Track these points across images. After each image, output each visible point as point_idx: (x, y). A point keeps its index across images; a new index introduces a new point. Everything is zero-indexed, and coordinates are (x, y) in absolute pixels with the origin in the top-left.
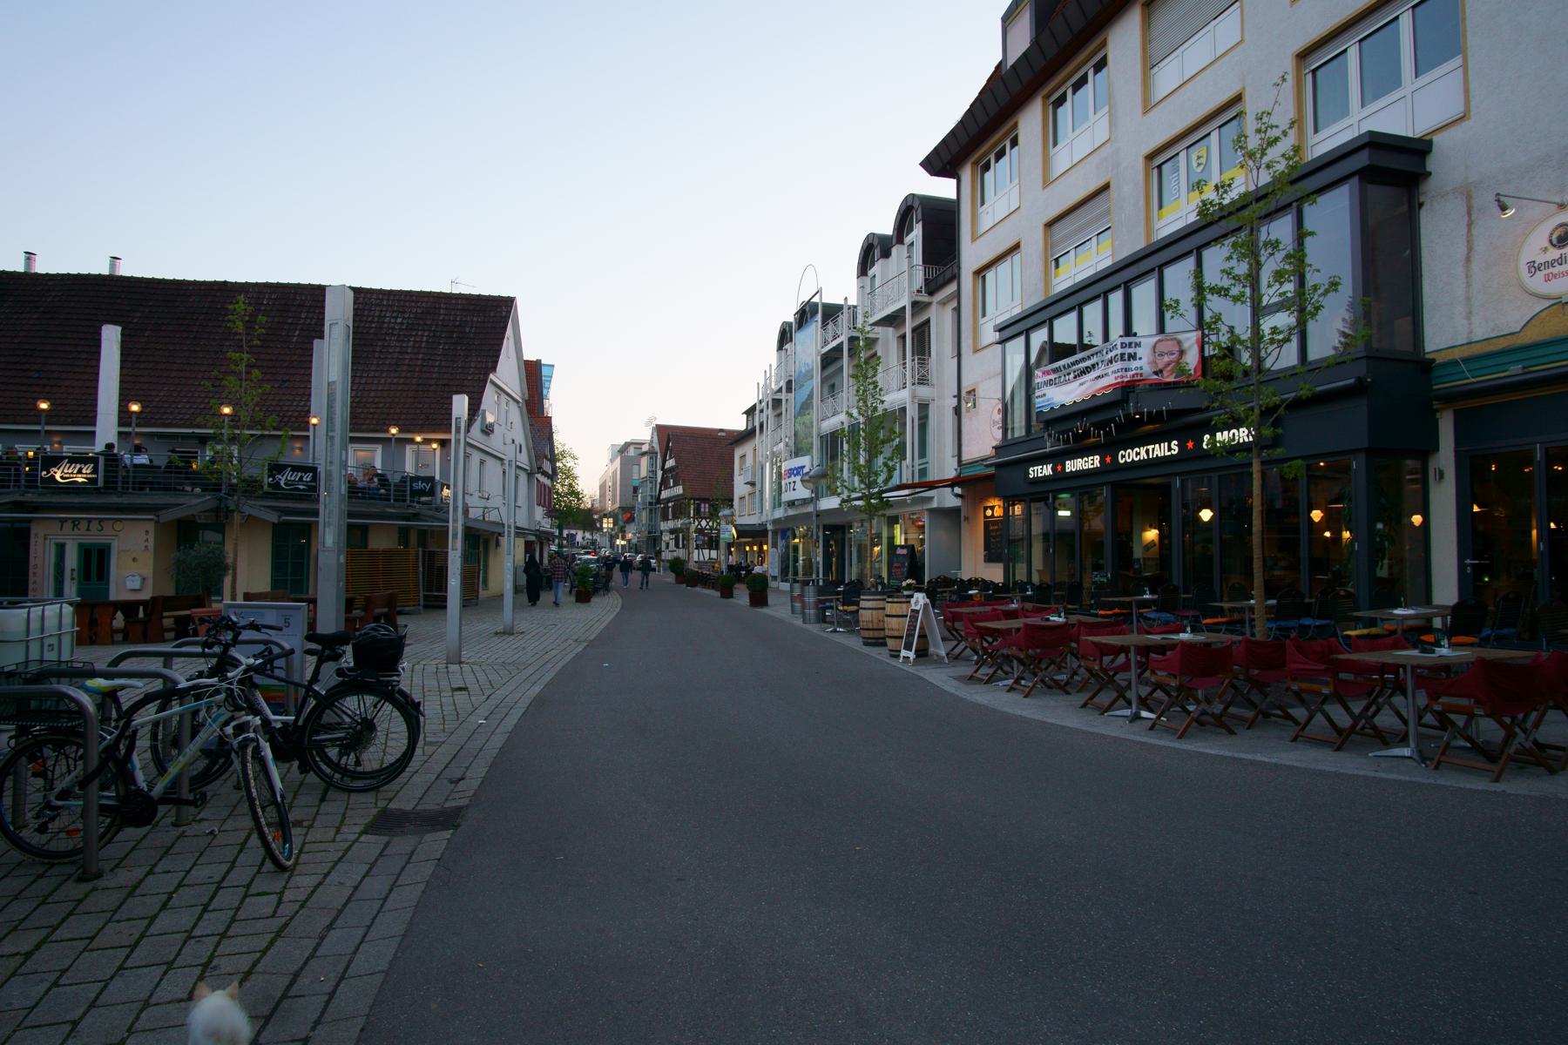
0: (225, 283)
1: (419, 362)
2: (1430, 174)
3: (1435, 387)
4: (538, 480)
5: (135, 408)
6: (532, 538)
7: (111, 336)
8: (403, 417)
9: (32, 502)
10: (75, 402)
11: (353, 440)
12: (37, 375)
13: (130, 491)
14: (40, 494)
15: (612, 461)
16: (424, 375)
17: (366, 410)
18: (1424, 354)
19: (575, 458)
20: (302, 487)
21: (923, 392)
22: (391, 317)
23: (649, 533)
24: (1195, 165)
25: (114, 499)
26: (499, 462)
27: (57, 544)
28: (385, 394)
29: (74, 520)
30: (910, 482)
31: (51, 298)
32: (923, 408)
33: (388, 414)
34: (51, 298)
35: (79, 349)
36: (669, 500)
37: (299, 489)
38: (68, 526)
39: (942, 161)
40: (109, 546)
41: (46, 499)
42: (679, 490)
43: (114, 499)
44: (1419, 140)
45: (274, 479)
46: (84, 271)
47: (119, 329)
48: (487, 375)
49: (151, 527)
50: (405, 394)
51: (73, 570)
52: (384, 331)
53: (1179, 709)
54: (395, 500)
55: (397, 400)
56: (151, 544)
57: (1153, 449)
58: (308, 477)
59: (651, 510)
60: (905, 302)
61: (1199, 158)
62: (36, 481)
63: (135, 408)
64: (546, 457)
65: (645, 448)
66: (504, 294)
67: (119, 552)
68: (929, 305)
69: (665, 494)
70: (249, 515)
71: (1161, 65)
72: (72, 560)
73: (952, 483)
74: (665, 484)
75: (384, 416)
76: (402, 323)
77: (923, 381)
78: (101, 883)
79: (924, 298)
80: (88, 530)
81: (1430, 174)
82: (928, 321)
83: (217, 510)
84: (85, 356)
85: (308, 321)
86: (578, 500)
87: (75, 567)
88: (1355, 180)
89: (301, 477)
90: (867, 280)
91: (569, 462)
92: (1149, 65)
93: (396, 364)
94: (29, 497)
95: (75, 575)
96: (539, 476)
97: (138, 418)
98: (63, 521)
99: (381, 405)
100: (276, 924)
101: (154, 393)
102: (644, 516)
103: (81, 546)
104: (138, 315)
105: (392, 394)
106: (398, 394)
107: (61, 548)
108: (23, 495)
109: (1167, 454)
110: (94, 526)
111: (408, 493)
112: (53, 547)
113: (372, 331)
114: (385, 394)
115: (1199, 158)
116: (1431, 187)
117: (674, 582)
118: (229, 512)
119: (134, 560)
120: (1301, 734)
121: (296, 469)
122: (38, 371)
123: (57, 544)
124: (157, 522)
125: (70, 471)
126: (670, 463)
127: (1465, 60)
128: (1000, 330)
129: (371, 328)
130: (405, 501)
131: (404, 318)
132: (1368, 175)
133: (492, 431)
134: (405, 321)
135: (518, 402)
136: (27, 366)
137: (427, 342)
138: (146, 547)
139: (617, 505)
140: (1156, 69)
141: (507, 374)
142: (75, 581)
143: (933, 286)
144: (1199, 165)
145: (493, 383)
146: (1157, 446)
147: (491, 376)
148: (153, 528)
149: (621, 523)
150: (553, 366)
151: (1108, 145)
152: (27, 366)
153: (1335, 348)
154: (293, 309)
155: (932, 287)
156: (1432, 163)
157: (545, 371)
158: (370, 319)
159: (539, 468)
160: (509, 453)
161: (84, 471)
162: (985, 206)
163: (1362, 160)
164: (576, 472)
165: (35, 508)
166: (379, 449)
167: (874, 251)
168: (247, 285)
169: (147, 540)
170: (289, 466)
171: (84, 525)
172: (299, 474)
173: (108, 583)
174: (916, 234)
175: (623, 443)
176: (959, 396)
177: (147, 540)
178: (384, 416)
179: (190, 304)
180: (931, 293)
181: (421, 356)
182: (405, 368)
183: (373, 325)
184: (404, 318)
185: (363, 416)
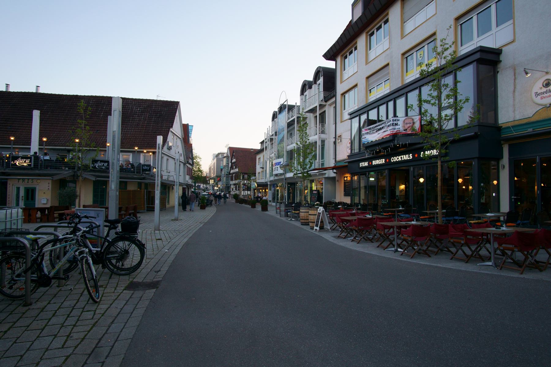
2: (501, 61)
3: (502, 136)
5: (45, 139)
6: (185, 186)
7: (36, 114)
8: (140, 143)
10: (23, 137)
11: (122, 151)
12: (10, 128)
15: (213, 159)
19: (200, 158)
20: (103, 168)
22: (136, 108)
24: (419, 57)
25: (37, 172)
26: (173, 160)
27: (17, 187)
29: (23, 179)
30: (318, 168)
32: (323, 142)
33: (134, 142)
34: (15, 101)
36: (233, 173)
37: (103, 169)
38: (21, 181)
39: (330, 55)
40: (35, 188)
42: (237, 170)
43: (37, 172)
44: (498, 49)
45: (94, 165)
47: (39, 111)
48: (169, 129)
49: (50, 182)
51: (22, 197)
54: (137, 173)
55: (137, 137)
56: (50, 188)
57: (403, 157)
58: (106, 164)
60: (317, 104)
61: (420, 55)
63: (45, 139)
64: (190, 158)
69: (232, 172)
71: (408, 22)
72: (22, 193)
73: (333, 168)
74: (232, 168)
76: (139, 110)
77: (323, 132)
81: (501, 61)
82: (325, 111)
85: (106, 109)
87: (23, 195)
88: (475, 63)
89: (104, 164)
90: (304, 97)
91: (198, 160)
96: (188, 165)
103: (25, 188)
104: (46, 106)
105: (136, 135)
107: (18, 189)
109: (408, 159)
110: (30, 181)
111: (141, 170)
112: (16, 188)
115: (420, 55)
116: (501, 66)
118: (78, 176)
119: (44, 193)
120: (454, 257)
121: (101, 161)
122: (10, 126)
123: (17, 187)
124: (52, 180)
125: (22, 162)
126: (234, 160)
127: (514, 21)
130: (140, 173)
131: (140, 108)
132: (480, 61)
133: (171, 149)
134: (141, 110)
135: (180, 139)
136: (6, 125)
138: (48, 189)
139: (215, 175)
141: (176, 129)
142: (23, 201)
143: (327, 99)
144: (420, 57)
145: (171, 132)
146: (405, 156)
147: (171, 129)
149: (216, 181)
150: (193, 126)
151: (389, 50)
152: (6, 125)
153: (467, 122)
155: (326, 99)
156: (502, 58)
157: (190, 128)
160: (177, 157)
161: (26, 162)
163: (477, 56)
164: (201, 163)
165: (9, 175)
166: (131, 155)
167: (306, 86)
169: (49, 186)
171: (26, 181)
172: (103, 163)
174: (321, 81)
175: (217, 153)
176: (335, 138)
177: (49, 186)
180: (326, 101)
183: (129, 111)
185: (125, 143)
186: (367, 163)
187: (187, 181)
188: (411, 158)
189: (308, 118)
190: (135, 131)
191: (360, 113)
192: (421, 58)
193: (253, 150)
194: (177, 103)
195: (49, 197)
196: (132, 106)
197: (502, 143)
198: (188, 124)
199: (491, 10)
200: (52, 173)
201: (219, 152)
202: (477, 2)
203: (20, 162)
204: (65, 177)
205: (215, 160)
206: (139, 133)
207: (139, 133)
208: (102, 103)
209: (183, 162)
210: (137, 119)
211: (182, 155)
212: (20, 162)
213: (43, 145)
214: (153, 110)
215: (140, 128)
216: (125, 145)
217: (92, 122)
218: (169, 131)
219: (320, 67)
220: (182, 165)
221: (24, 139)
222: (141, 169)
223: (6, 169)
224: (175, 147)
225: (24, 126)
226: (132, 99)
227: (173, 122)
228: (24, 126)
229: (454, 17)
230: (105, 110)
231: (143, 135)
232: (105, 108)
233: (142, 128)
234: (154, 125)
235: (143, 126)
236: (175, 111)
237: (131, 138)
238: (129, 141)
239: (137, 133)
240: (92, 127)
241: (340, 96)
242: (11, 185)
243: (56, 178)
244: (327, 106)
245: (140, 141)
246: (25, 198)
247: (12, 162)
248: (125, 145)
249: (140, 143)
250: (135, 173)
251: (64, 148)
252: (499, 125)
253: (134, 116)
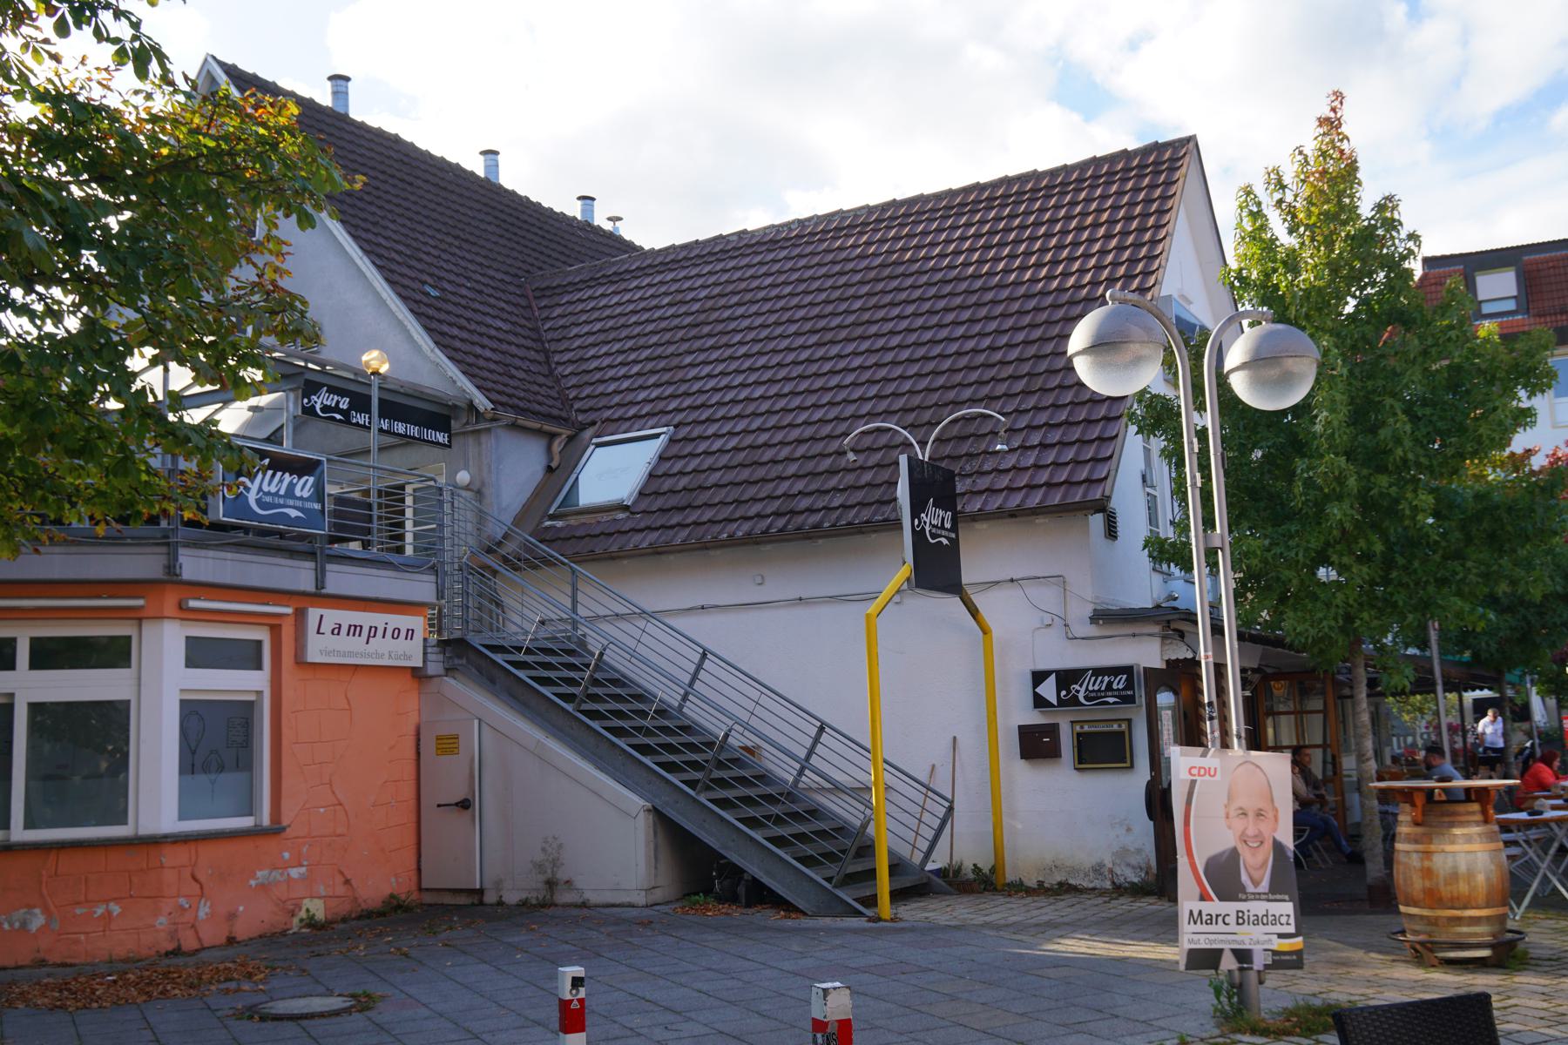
45: (1069, 692)
89: (1110, 684)
121: (1099, 672)
125: (1096, 688)
161: (1115, 687)
170: (324, 385)
172: (1106, 679)
194: (1190, 142)
203: (1091, 688)
212: (1091, 688)
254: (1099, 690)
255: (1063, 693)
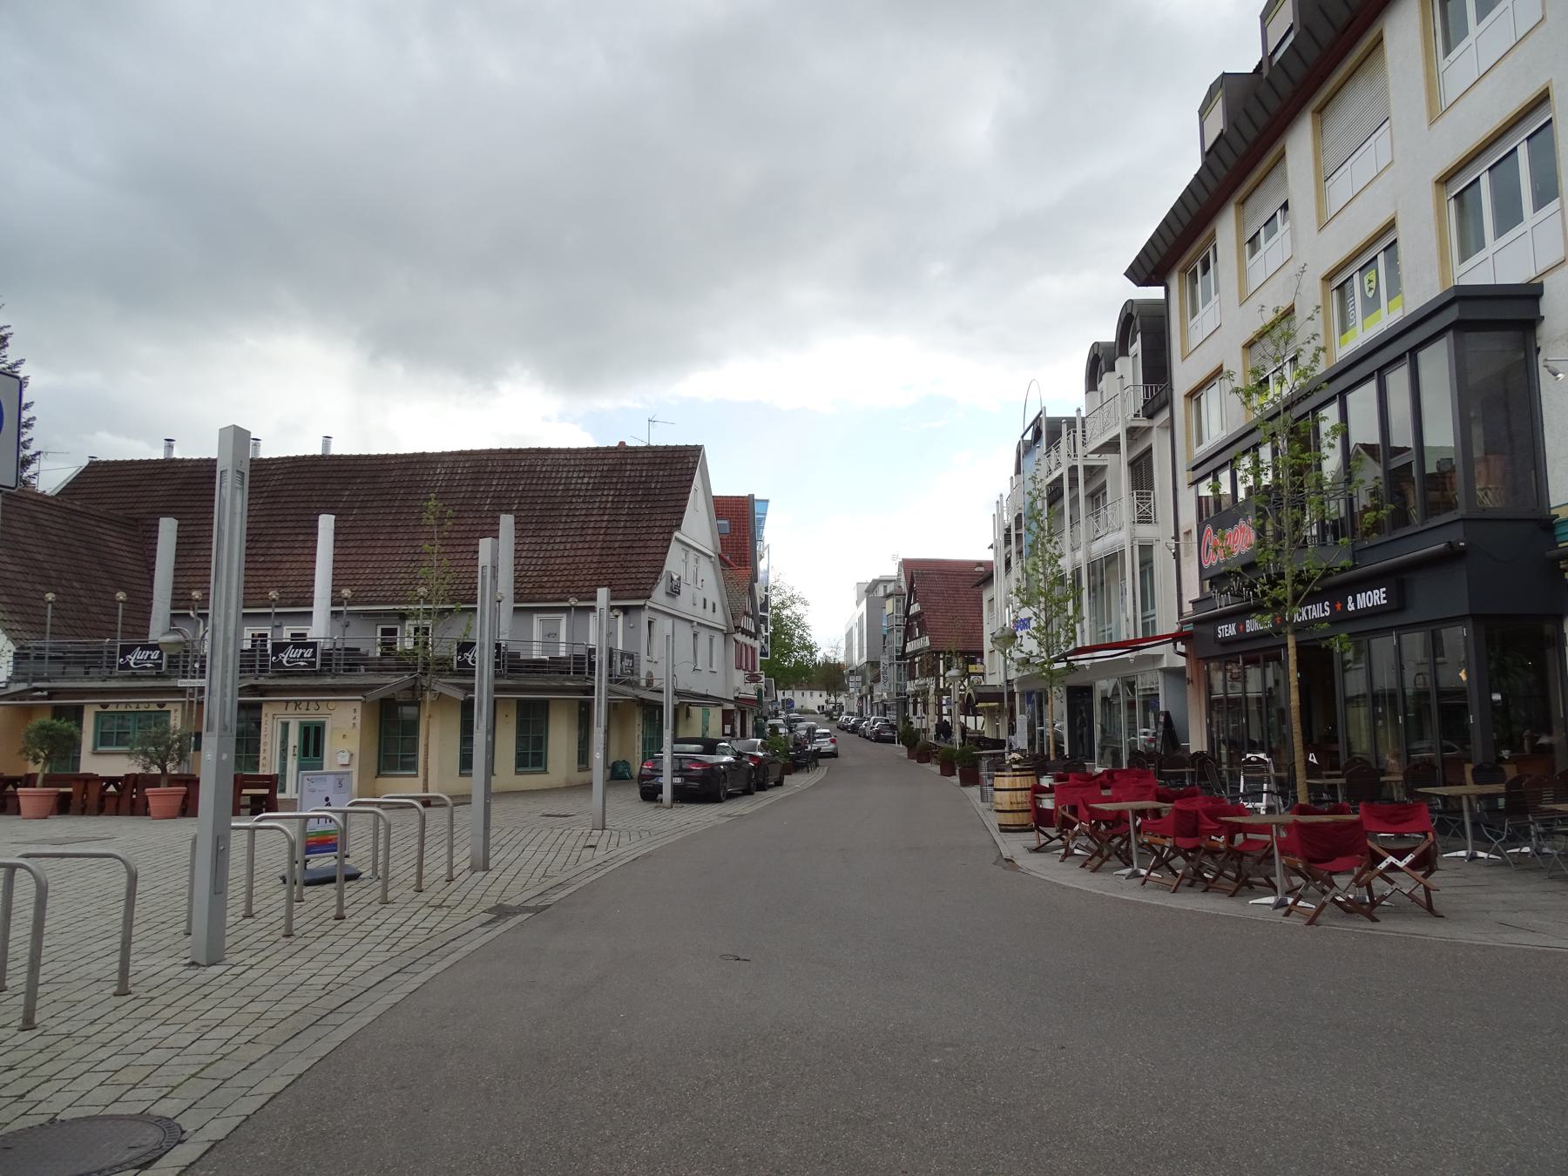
0: (424, 454)
1: (604, 524)
2: (1543, 317)
3: (1560, 545)
4: (736, 641)
6: (731, 707)
7: (326, 523)
8: (587, 583)
9: (265, 685)
10: (293, 584)
12: (262, 559)
13: (342, 672)
14: (270, 678)
15: (858, 604)
16: (608, 538)
17: (551, 579)
18: (1550, 509)
19: (805, 603)
20: (302, 664)
21: (1145, 531)
22: (578, 477)
23: (898, 694)
24: (1367, 289)
25: (329, 681)
27: (282, 723)
28: (571, 560)
29: (296, 701)
30: (1132, 638)
31: (273, 483)
32: (1146, 550)
33: (573, 581)
34: (273, 483)
35: (298, 531)
36: (915, 653)
37: (146, 668)
38: (292, 706)
39: (1148, 268)
40: (323, 724)
41: (271, 682)
42: (925, 642)
43: (329, 681)
44: (1528, 285)
45: (277, 657)
46: (301, 453)
47: (333, 517)
48: (671, 533)
49: (358, 706)
50: (589, 559)
51: (295, 747)
52: (571, 493)
53: (1262, 880)
54: (574, 673)
55: (581, 566)
56: (358, 721)
57: (1311, 609)
59: (899, 665)
60: (1119, 430)
61: (1370, 281)
62: (268, 666)
64: (746, 614)
65: (891, 588)
66: (692, 443)
67: (332, 730)
68: (1150, 428)
69: (910, 647)
70: (440, 693)
71: (1334, 177)
72: (294, 739)
73: (1175, 638)
74: (908, 635)
75: (569, 584)
76: (588, 483)
77: (1145, 519)
78: (345, 921)
79: (1143, 423)
80: (307, 709)
81: (1543, 317)
82: (1149, 450)
83: (413, 688)
84: (301, 538)
85: (499, 488)
86: (811, 655)
87: (296, 744)
88: (1451, 333)
89: (303, 653)
90: (1096, 395)
91: (798, 609)
92: (1323, 178)
93: (582, 528)
94: (262, 681)
95: (296, 753)
96: (739, 637)
97: (54, 608)
98: (287, 702)
99: (566, 572)
100: (427, 936)
101: (361, 571)
102: (892, 673)
103: (301, 723)
104: (347, 493)
105: (577, 559)
106: (583, 559)
107: (286, 726)
108: (256, 679)
109: (1322, 615)
110: (312, 706)
111: (587, 665)
112: (280, 725)
113: (559, 494)
114: (571, 560)
115: (1370, 281)
116: (1546, 331)
117: (906, 756)
118: (423, 689)
120: (1089, 862)
122: (263, 555)
123: (282, 723)
124: (364, 702)
125: (141, 658)
126: (915, 608)
127: (1562, 203)
128: (1194, 469)
129: (558, 490)
131: (590, 477)
132: (1460, 327)
133: (679, 593)
134: (592, 481)
135: (710, 557)
137: (612, 501)
138: (354, 724)
139: (865, 659)
140: (1330, 181)
141: (697, 527)
142: (296, 757)
143: (1150, 410)
144: (1370, 289)
145: (678, 540)
146: (1314, 606)
147: (677, 534)
148: (360, 708)
149: (869, 682)
150: (767, 501)
151: (1291, 262)
154: (486, 476)
155: (1150, 410)
156: (1546, 306)
158: (557, 481)
159: (737, 628)
160: (699, 613)
162: (1196, 318)
163: (1452, 315)
164: (807, 620)
167: (1099, 363)
168: (443, 454)
170: (138, 646)
171: (303, 706)
172: (301, 651)
173: (322, 759)
174: (1136, 348)
175: (870, 581)
176: (1176, 538)
178: (569, 584)
179: (392, 479)
180: (1150, 417)
181: (606, 518)
182: (590, 531)
183: (561, 488)
184: (590, 477)
185: (549, 585)
186: (1234, 625)
187: (738, 689)
188: (1327, 614)
189: (1108, 469)
190: (575, 546)
191: (1216, 465)
192: (1373, 291)
193: (982, 569)
195: (356, 749)
196: (569, 471)
197: (1562, 566)
198: (752, 496)
199: (1517, 157)
200: (362, 682)
201: (877, 577)
202: (1480, 137)
203: (291, 656)
204: (393, 694)
205: (864, 604)
206: (585, 552)
207: (585, 552)
208: (488, 469)
209: (722, 630)
210: (582, 509)
211: (718, 607)
213: (341, 604)
214: (626, 480)
215: (588, 538)
216: (547, 591)
217: (462, 528)
218: (670, 540)
219: (1132, 301)
220: (719, 639)
221: (295, 589)
222: (587, 661)
223: (261, 676)
224: (693, 585)
225: (295, 551)
226: (569, 451)
227: (683, 513)
228: (295, 551)
229: (1432, 178)
230: (495, 491)
231: (597, 552)
232: (497, 485)
233: (594, 538)
234: (628, 524)
235: (597, 532)
236: (688, 477)
237: (565, 569)
238: (558, 578)
239: (579, 552)
240: (463, 542)
241: (1182, 398)
242: (270, 716)
243: (375, 695)
244: (1155, 431)
245: (589, 578)
246: (299, 751)
247: (274, 658)
248: (547, 591)
249: (587, 583)
250: (569, 673)
251: (391, 607)
252: (1553, 512)
253: (574, 500)
254: (296, 658)
255: (274, 658)
